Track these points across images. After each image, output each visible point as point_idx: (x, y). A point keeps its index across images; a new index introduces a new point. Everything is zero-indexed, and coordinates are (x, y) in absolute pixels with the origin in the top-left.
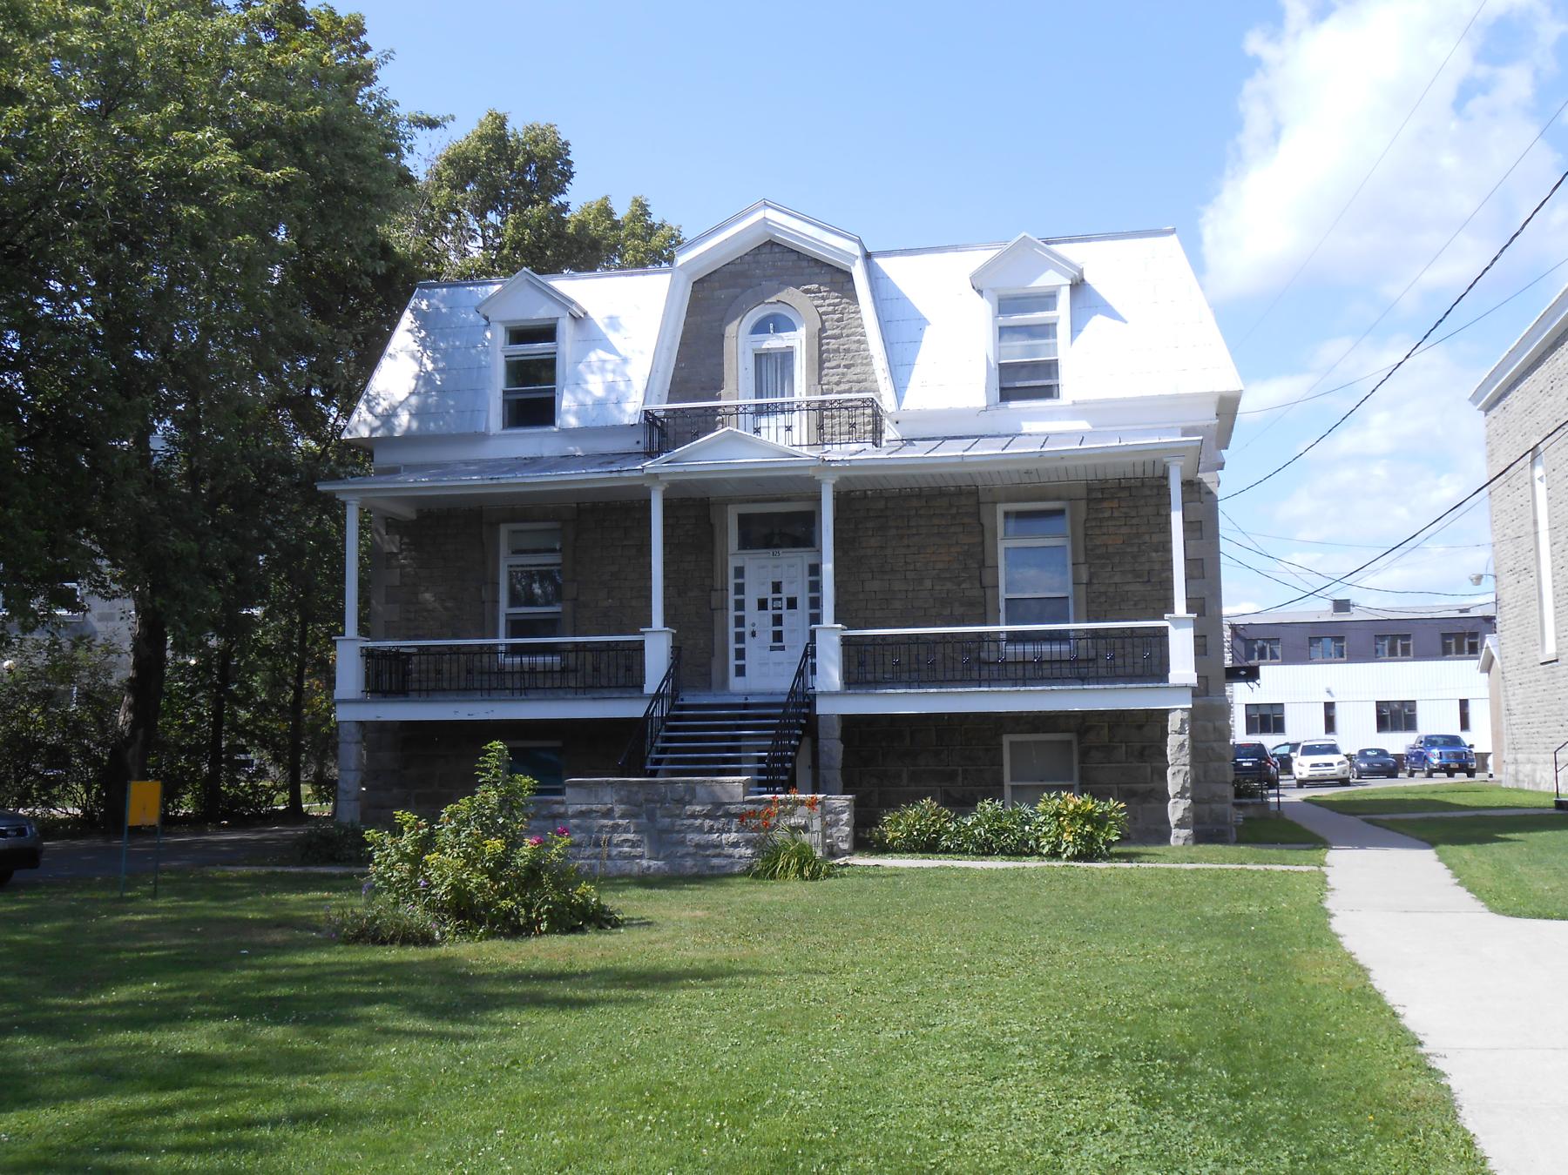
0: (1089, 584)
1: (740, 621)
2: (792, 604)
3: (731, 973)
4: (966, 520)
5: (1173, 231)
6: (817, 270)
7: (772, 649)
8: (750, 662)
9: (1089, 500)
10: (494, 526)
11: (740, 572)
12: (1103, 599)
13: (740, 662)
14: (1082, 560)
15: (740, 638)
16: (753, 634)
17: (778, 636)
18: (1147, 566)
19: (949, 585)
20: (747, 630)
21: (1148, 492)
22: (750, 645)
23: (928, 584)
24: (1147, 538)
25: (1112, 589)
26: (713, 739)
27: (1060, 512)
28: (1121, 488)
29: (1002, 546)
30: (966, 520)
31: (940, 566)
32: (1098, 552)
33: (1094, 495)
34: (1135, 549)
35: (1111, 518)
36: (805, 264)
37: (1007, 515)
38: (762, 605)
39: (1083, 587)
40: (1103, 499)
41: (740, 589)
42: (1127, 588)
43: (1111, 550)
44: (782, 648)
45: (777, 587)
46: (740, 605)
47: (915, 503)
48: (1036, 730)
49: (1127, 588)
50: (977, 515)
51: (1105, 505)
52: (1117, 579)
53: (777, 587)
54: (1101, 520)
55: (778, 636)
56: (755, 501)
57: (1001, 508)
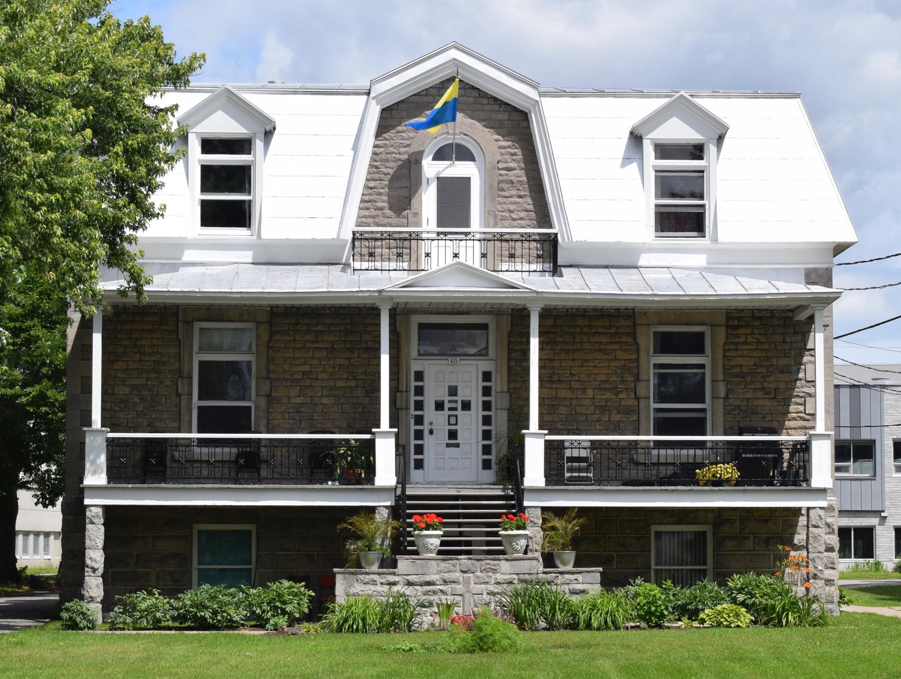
0: (726, 398)
1: (419, 420)
2: (466, 406)
3: (855, 589)
4: (624, 339)
5: (797, 96)
6: (496, 107)
7: (448, 445)
8: (428, 456)
9: (728, 327)
10: (189, 323)
11: (419, 376)
12: (736, 412)
13: (419, 457)
14: (721, 377)
15: (419, 435)
16: (431, 432)
17: (453, 435)
18: (773, 386)
19: (608, 395)
20: (426, 428)
21: (775, 322)
22: (429, 442)
23: (590, 393)
24: (774, 361)
25: (744, 404)
26: (458, 516)
27: (484, 327)
28: (754, 318)
29: (197, 359)
30: (624, 339)
31: (602, 377)
32: (734, 371)
33: (731, 323)
34: (765, 370)
35: (745, 343)
36: (485, 101)
37: (422, 326)
38: (439, 406)
39: (722, 401)
40: (739, 327)
41: (419, 391)
42: (756, 403)
43: (745, 370)
44: (457, 445)
45: (453, 391)
46: (419, 406)
47: (580, 322)
48: (680, 522)
49: (756, 403)
50: (634, 335)
51: (741, 331)
52: (749, 395)
53: (453, 391)
54: (736, 344)
55: (453, 435)
56: (459, 313)
57: (416, 320)
